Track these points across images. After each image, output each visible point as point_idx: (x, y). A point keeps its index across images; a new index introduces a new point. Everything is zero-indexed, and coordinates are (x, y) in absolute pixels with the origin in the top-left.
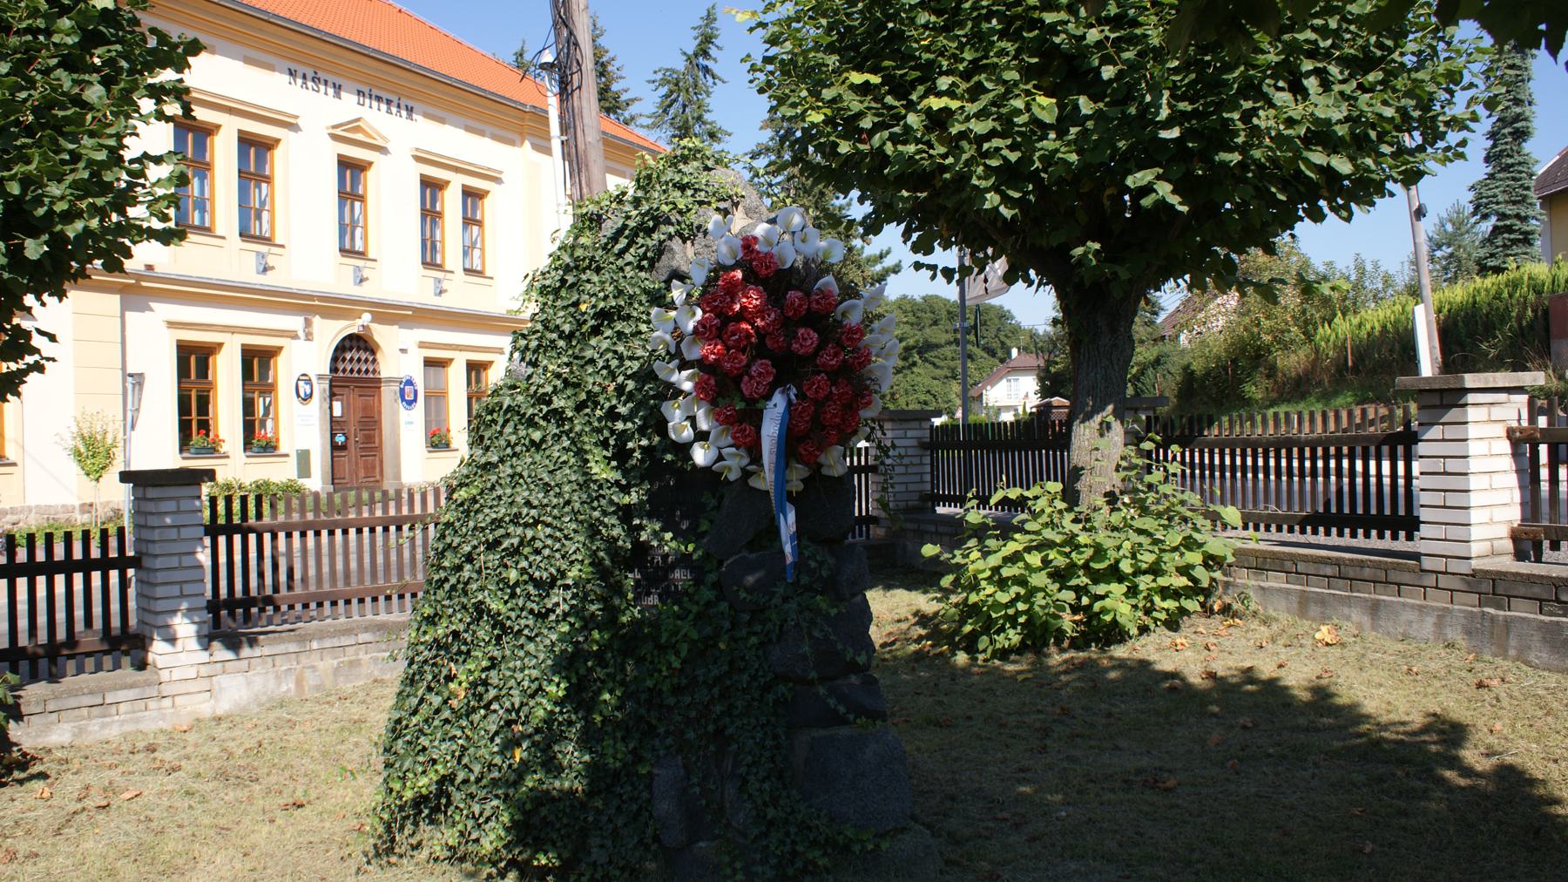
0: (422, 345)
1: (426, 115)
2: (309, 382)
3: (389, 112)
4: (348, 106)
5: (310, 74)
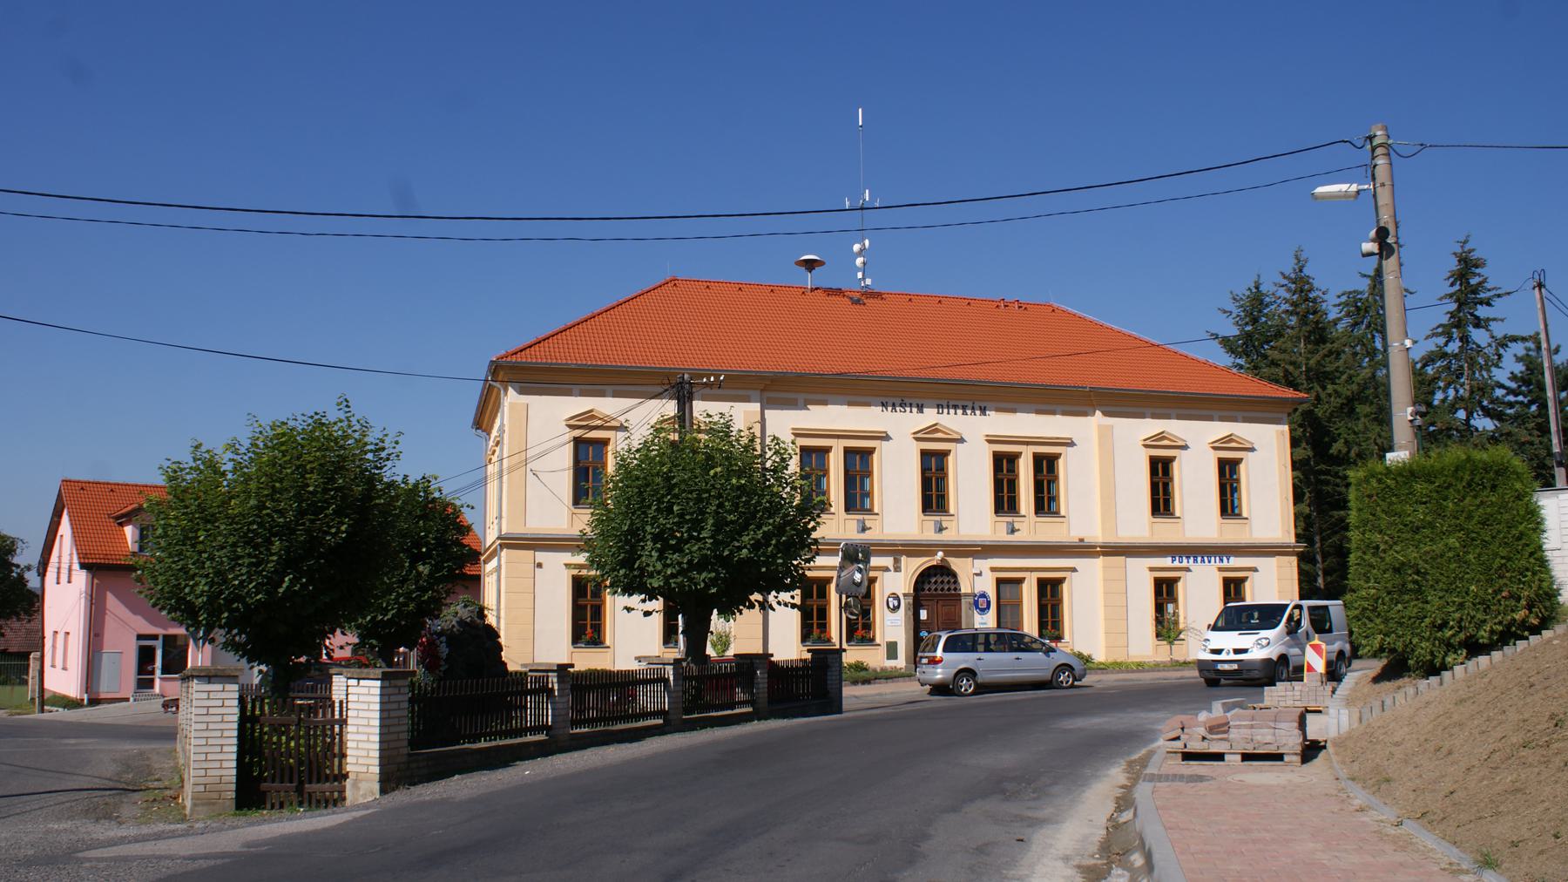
0: (993, 569)
1: (997, 410)
2: (898, 598)
3: (964, 413)
4: (930, 416)
5: (898, 401)
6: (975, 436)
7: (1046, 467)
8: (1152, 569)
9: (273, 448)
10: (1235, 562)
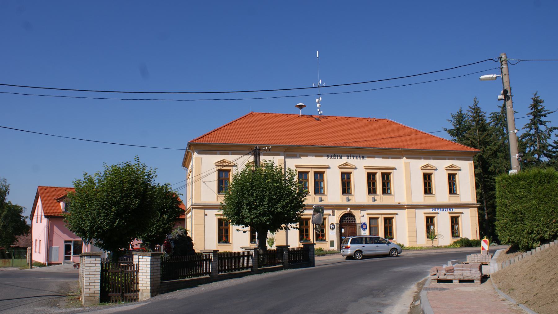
7: (386, 177)
8: (425, 213)
10: (455, 210)
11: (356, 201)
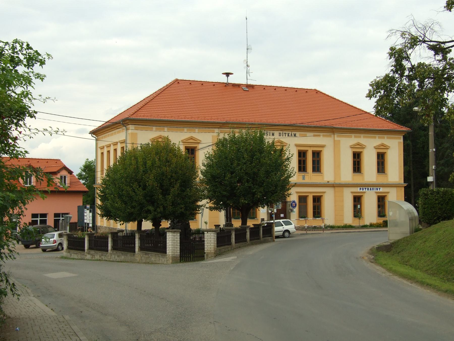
0: (297, 193)
6: (271, 132)
7: (317, 155)
8: (352, 192)
9: (246, 173)
10: (382, 190)
11: (342, 180)
